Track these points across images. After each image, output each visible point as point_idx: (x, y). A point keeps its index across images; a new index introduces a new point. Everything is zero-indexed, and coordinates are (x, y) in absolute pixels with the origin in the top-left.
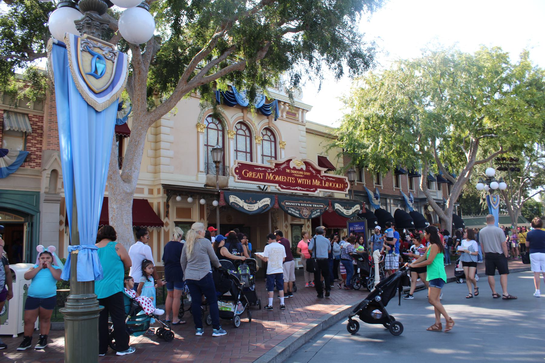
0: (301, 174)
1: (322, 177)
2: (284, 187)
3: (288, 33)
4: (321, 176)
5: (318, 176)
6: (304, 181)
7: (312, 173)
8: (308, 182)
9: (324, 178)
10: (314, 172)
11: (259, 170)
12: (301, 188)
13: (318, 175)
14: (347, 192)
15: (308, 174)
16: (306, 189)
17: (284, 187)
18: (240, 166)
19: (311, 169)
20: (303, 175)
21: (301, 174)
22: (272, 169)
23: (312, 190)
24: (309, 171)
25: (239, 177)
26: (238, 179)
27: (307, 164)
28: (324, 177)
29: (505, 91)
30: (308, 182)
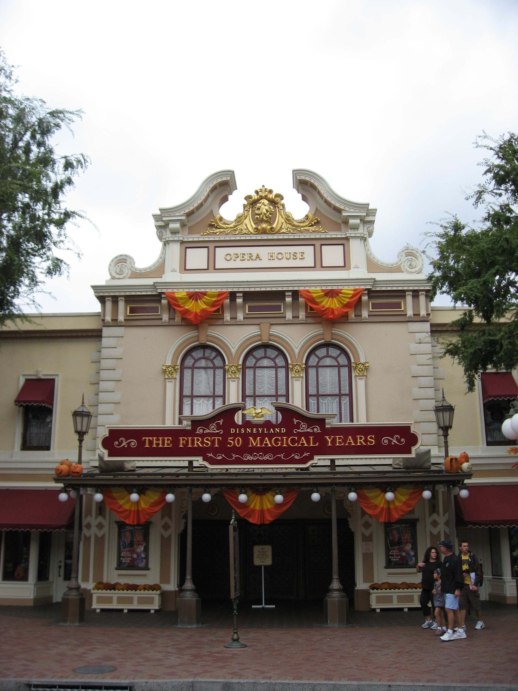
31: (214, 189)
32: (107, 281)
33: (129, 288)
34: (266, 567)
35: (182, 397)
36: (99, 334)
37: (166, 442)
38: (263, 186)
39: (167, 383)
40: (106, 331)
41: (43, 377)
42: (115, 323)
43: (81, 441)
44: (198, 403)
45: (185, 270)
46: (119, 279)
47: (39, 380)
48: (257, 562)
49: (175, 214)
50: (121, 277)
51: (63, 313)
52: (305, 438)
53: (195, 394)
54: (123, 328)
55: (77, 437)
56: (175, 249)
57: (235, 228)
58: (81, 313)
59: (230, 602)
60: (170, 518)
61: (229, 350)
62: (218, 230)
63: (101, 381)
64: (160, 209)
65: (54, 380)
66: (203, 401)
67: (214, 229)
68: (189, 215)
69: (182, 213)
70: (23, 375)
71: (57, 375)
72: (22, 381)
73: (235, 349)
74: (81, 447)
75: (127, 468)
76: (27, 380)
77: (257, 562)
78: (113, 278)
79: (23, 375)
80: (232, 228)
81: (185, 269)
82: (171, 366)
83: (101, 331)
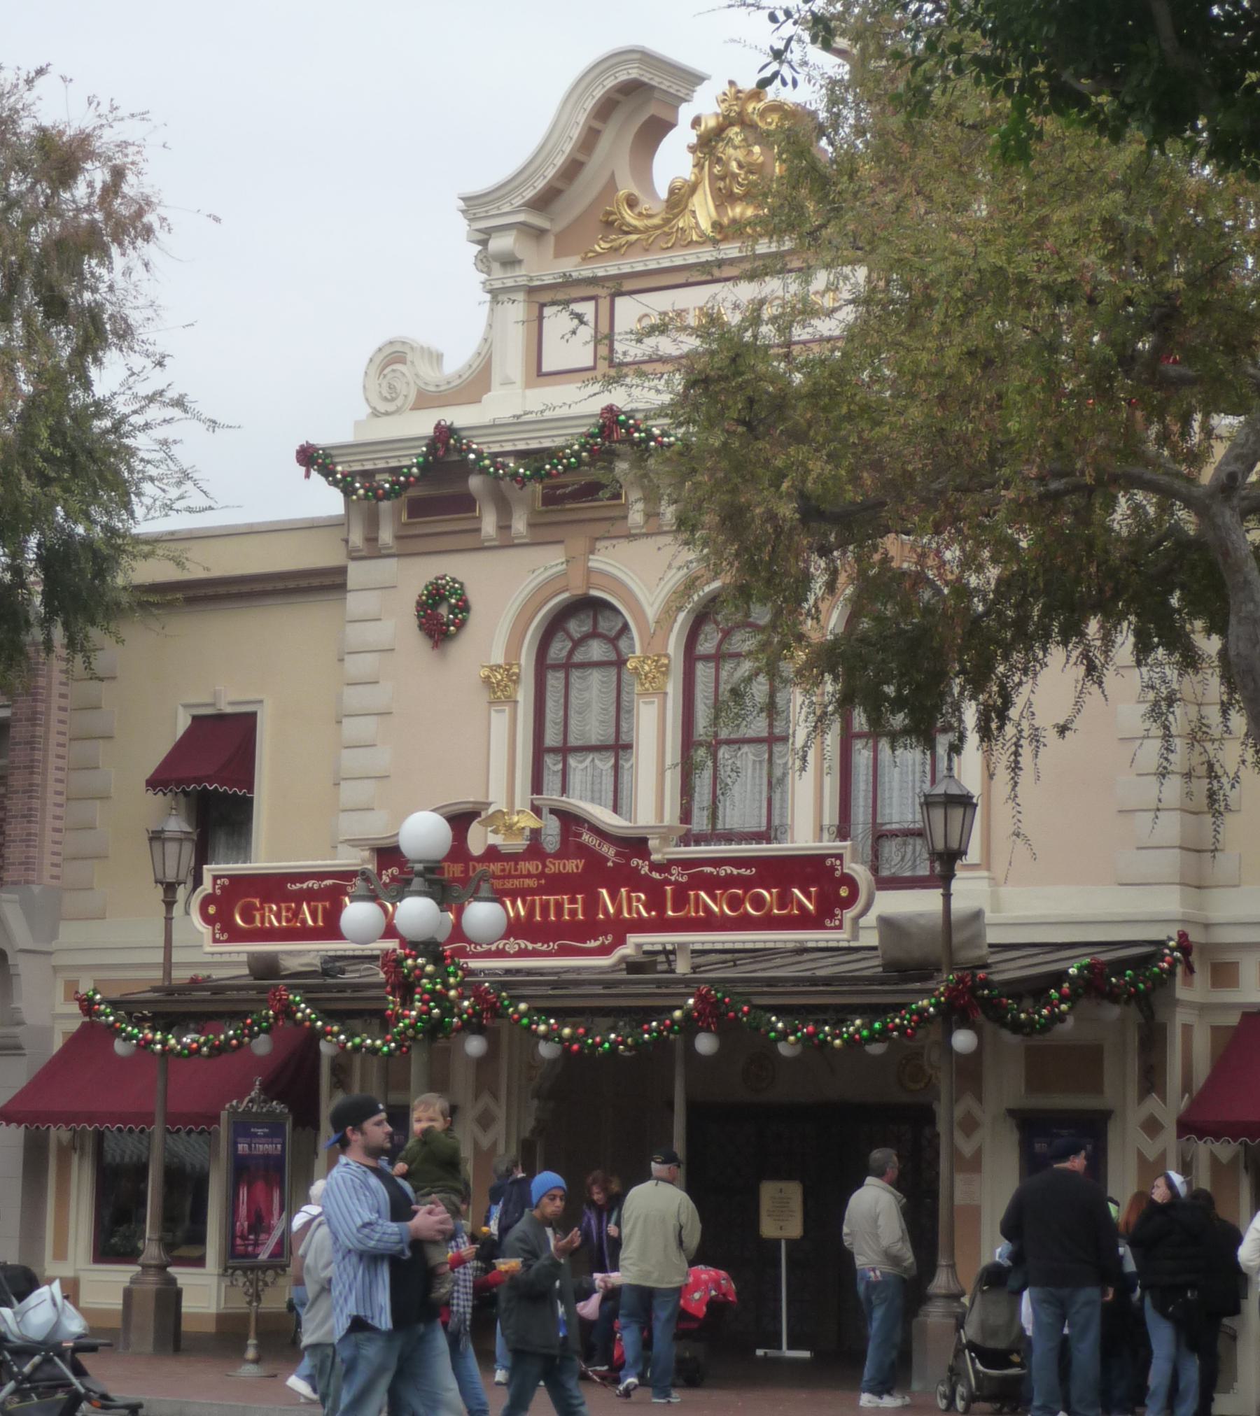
0: (529, 876)
1: (664, 867)
2: (708, 869)
3: (847, 1241)
4: (654, 867)
5: (637, 869)
6: (545, 907)
7: (599, 860)
8: (573, 907)
9: (676, 874)
10: (609, 851)
11: (310, 890)
12: (523, 943)
13: (635, 862)
14: (64, 653)
15: (573, 866)
16: (553, 946)
17: (708, 869)
18: (223, 887)
19: (587, 838)
20: (542, 875)
21: (529, 876)
22: (364, 875)
23: (592, 944)
24: (584, 851)
25: (222, 931)
26: (215, 941)
27: (120, 641)
28: (675, 870)
29: (1006, 728)
30: (573, 907)
31: (606, 109)
32: (357, 424)
33: (390, 446)
34: (790, 1242)
35: (539, 751)
36: (338, 581)
37: (284, 914)
38: (732, 83)
39: (493, 714)
40: (357, 573)
41: (229, 710)
42: (373, 550)
43: (169, 904)
44: (581, 766)
45: (540, 374)
46: (387, 414)
47: (221, 718)
48: (768, 1229)
49: (498, 208)
50: (391, 407)
51: (290, 521)
52: (584, 900)
53: (573, 741)
54: (394, 561)
55: (160, 890)
56: (516, 310)
57: (666, 229)
58: (313, 519)
59: (259, 1335)
60: (495, 1097)
61: (643, 613)
62: (624, 239)
63: (346, 716)
64: (464, 199)
65: (253, 716)
66: (593, 760)
67: (614, 236)
68: (544, 201)
69: (518, 201)
70: (186, 706)
71: (261, 702)
72: (183, 723)
73: (656, 606)
74: (171, 919)
75: (286, 969)
76: (195, 718)
77: (768, 1229)
78: (376, 414)
79: (186, 706)
80: (657, 227)
81: (539, 374)
82: (500, 667)
83: (342, 571)
